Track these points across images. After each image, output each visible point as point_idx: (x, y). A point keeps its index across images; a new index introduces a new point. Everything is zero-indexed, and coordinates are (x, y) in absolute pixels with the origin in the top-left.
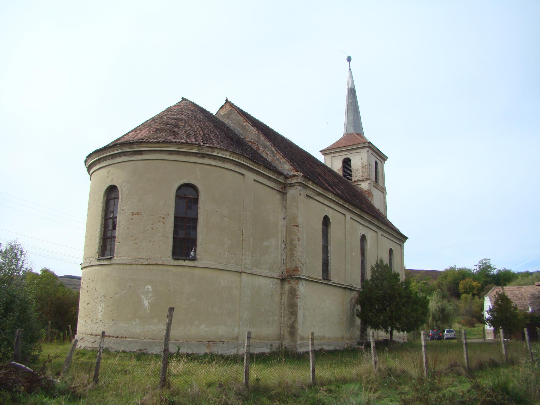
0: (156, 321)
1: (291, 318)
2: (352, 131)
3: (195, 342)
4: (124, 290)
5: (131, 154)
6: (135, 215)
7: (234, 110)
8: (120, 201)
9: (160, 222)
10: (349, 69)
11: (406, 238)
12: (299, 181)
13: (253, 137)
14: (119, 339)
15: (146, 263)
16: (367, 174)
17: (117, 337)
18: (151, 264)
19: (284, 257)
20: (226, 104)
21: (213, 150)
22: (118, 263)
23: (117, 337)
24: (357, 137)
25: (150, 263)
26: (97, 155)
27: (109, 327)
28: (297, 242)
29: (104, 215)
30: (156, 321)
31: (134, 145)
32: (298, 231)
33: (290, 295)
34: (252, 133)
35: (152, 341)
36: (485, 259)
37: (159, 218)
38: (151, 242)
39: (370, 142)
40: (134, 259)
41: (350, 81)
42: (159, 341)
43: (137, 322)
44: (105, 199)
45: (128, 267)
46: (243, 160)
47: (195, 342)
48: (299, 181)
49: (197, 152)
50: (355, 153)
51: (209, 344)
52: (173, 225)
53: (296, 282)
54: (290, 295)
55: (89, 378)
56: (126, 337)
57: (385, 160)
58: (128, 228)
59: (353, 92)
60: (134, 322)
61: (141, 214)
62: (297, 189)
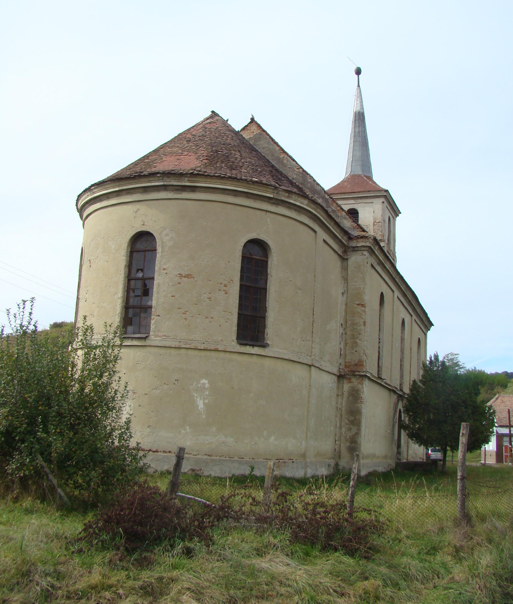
0: (214, 429)
1: (351, 429)
2: (359, 171)
3: (262, 460)
4: (168, 384)
5: (177, 190)
6: (183, 278)
7: (265, 134)
8: (158, 255)
9: (220, 290)
10: (357, 85)
11: (431, 324)
12: (368, 244)
13: (295, 176)
14: (159, 453)
15: (202, 348)
16: (380, 233)
17: (157, 451)
18: (208, 349)
19: (342, 346)
20: (252, 124)
21: (291, 195)
22: (158, 345)
23: (157, 451)
24: (367, 181)
25: (207, 348)
26: (117, 184)
27: (142, 436)
28: (362, 327)
29: (127, 273)
30: (214, 429)
31: (185, 177)
32: (365, 312)
33: (350, 398)
34: (294, 170)
35: (209, 457)
36: (452, 354)
37: (219, 284)
38: (208, 318)
39: (387, 191)
40: (183, 341)
41: (358, 102)
42: (218, 458)
43: (188, 431)
44: (129, 250)
45: (173, 351)
46: (318, 213)
47: (262, 460)
48: (368, 245)
49: (272, 196)
50: (365, 203)
51: (280, 463)
52: (238, 296)
53: (359, 381)
54: (350, 398)
55: (268, 509)
56: (170, 452)
57: (397, 215)
58: (172, 296)
59: (362, 117)
60: (183, 431)
61: (194, 277)
62: (363, 254)
